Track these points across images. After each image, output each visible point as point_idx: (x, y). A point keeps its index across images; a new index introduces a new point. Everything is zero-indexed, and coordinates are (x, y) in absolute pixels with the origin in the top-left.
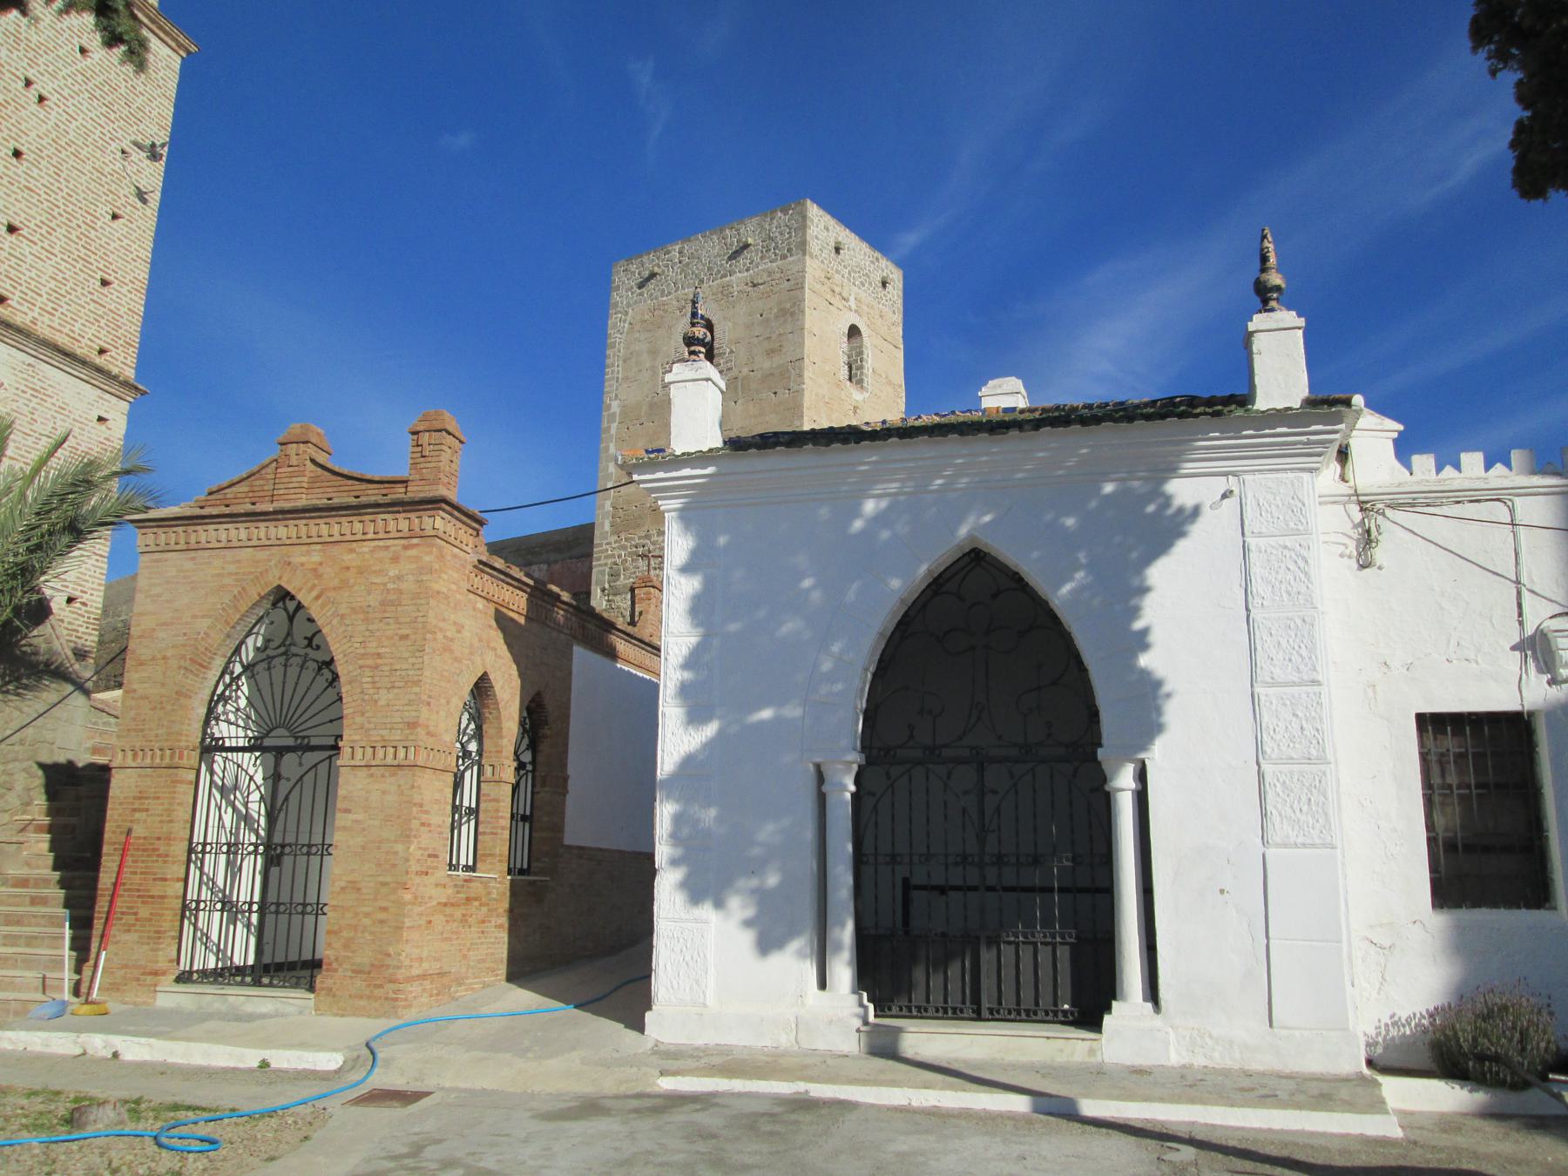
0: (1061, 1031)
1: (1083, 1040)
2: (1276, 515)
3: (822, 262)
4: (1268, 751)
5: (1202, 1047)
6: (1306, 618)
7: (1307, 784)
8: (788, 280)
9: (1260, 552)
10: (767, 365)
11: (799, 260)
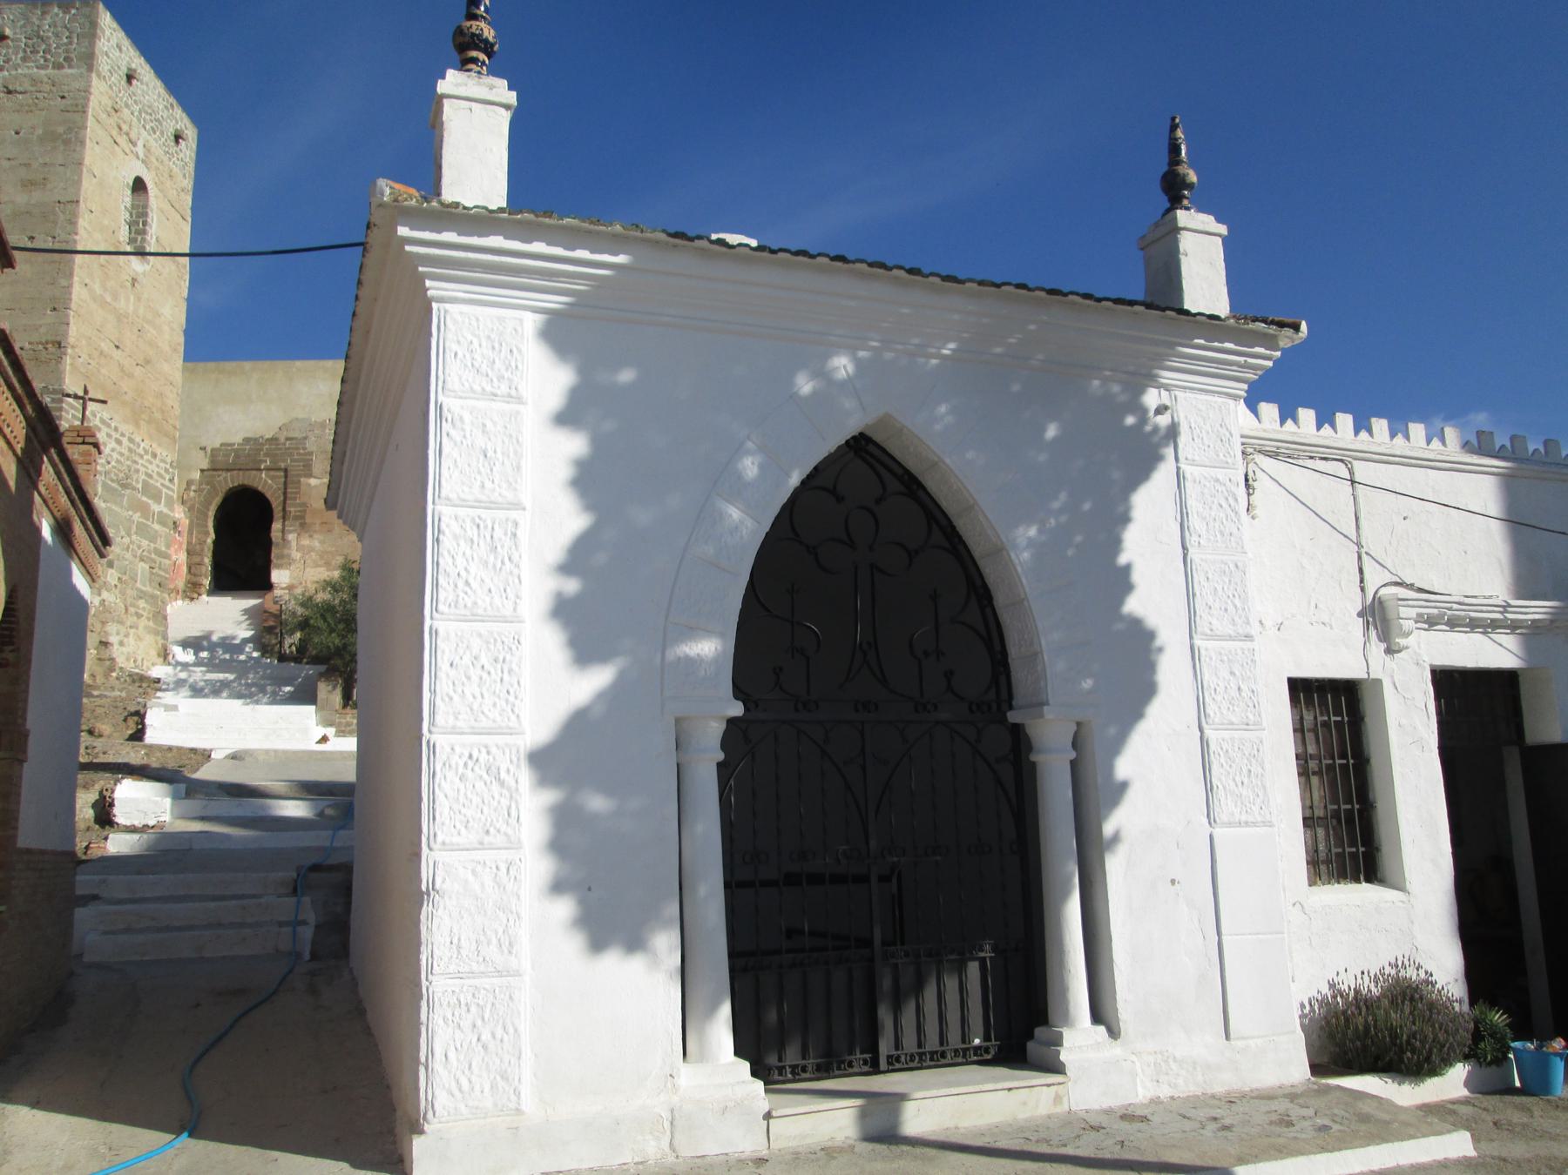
0: (1018, 1079)
1: (1049, 1085)
2: (1207, 442)
3: (111, 87)
4: (1212, 715)
5: (1167, 1074)
6: (1239, 564)
7: (1247, 754)
8: (63, 97)
9: (1195, 481)
10: (21, 199)
11: (81, 75)
